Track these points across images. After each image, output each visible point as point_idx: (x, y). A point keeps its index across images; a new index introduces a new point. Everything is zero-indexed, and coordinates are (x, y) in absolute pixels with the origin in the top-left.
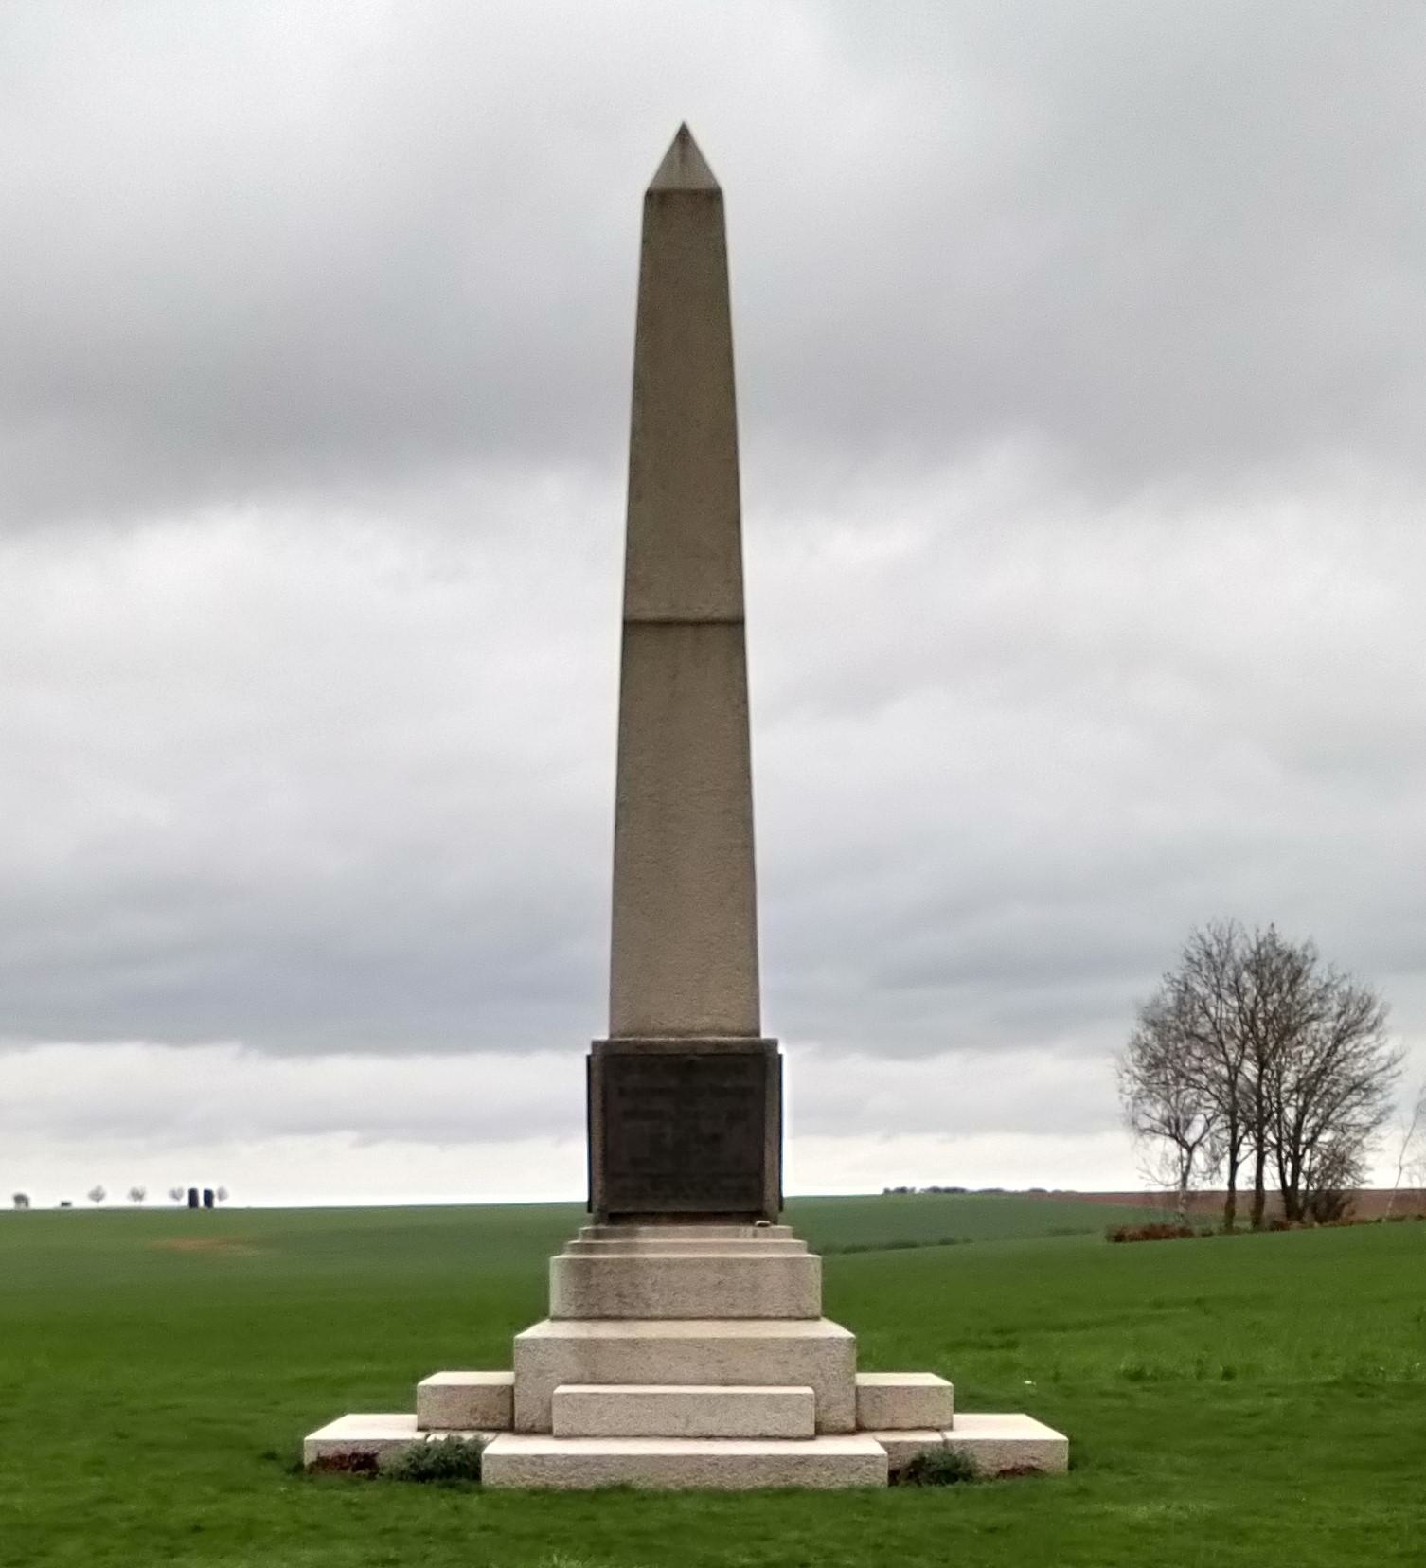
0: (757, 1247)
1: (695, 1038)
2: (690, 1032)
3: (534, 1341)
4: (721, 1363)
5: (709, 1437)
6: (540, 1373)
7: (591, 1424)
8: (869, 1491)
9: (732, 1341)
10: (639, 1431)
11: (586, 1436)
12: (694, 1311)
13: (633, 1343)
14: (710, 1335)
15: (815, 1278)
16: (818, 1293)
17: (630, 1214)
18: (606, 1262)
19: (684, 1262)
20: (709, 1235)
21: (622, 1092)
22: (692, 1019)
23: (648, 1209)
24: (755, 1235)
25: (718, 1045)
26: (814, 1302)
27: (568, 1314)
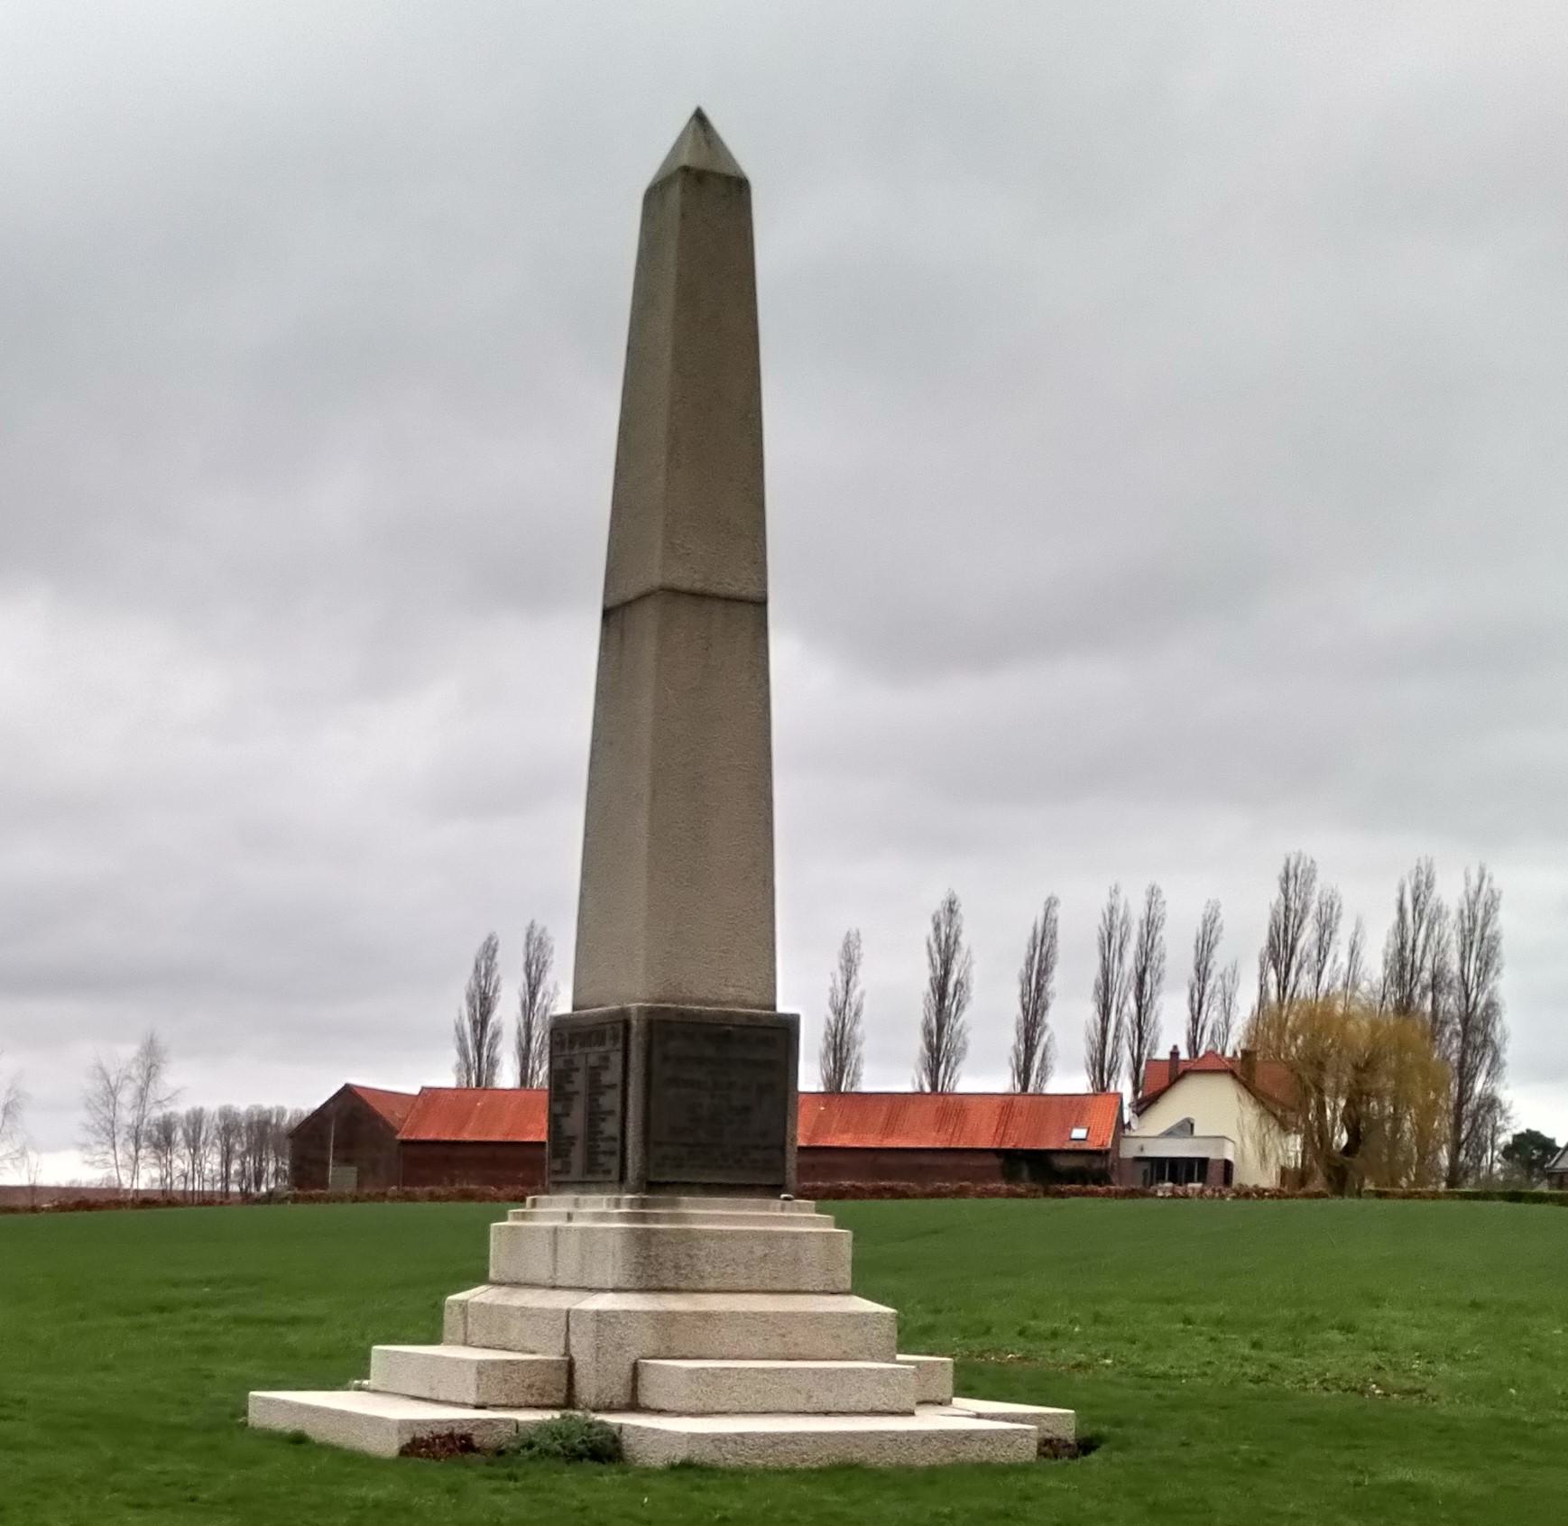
0: (791, 1220)
1: (689, 1007)
2: (684, 1001)
3: (463, 1306)
4: (782, 1337)
5: (827, 1413)
6: (620, 1347)
7: (723, 1399)
8: (1030, 1463)
9: (793, 1315)
10: (765, 1407)
11: (718, 1413)
12: (743, 1283)
13: (707, 1316)
14: (625, 1307)
15: (846, 1251)
16: (848, 1268)
17: (667, 1184)
18: (664, 1232)
19: (733, 1234)
20: (743, 1208)
21: (666, 1058)
22: (711, 989)
23: (684, 1180)
24: (783, 1209)
25: (750, 1017)
26: (845, 1276)
27: (628, 1286)
